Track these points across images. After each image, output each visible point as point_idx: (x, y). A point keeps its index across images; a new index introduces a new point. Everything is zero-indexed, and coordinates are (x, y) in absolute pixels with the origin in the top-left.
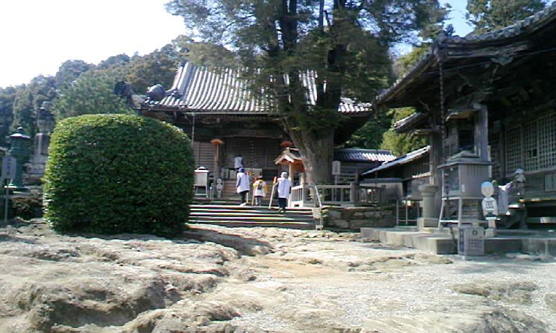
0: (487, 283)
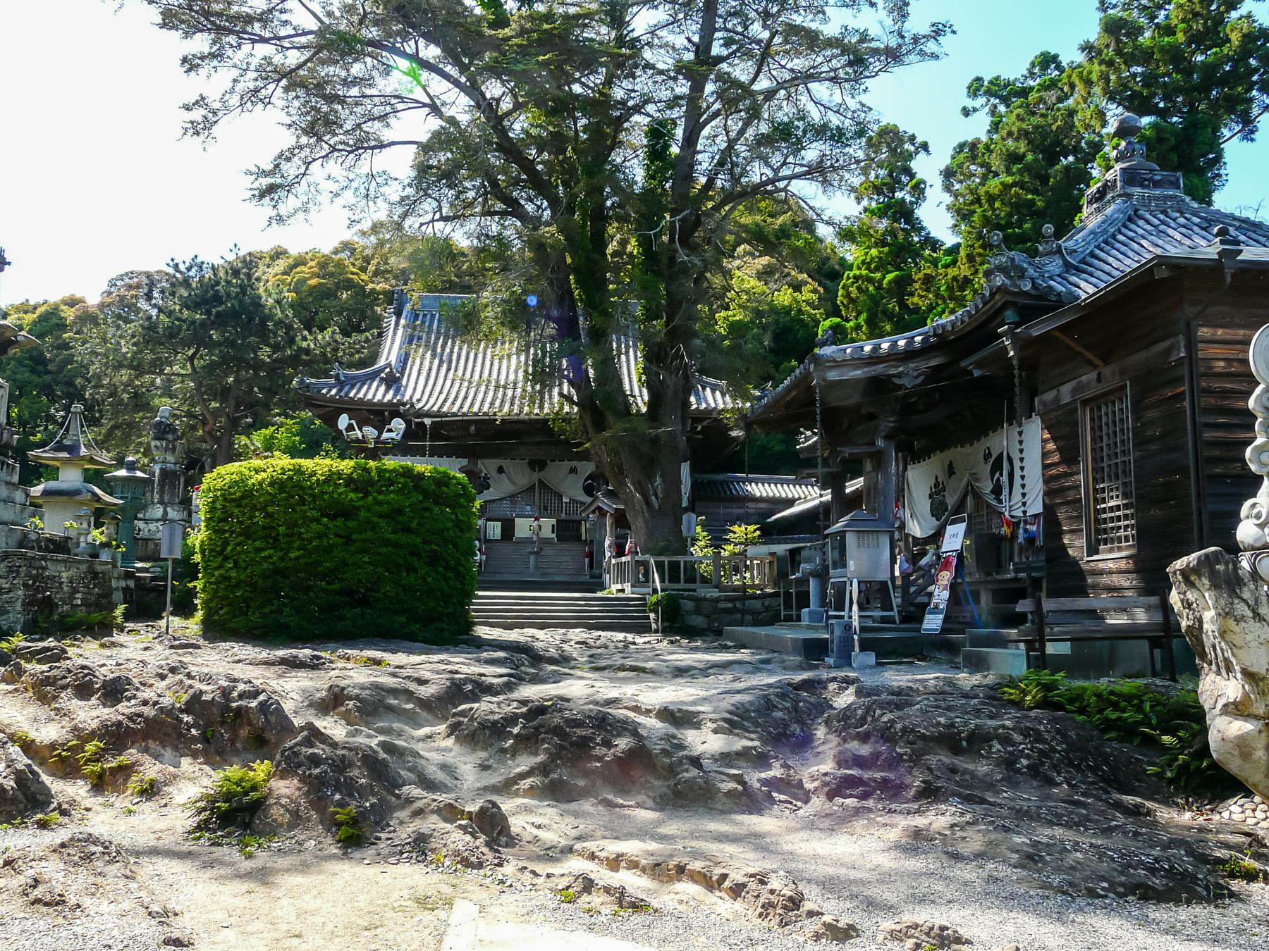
0: (247, 865)
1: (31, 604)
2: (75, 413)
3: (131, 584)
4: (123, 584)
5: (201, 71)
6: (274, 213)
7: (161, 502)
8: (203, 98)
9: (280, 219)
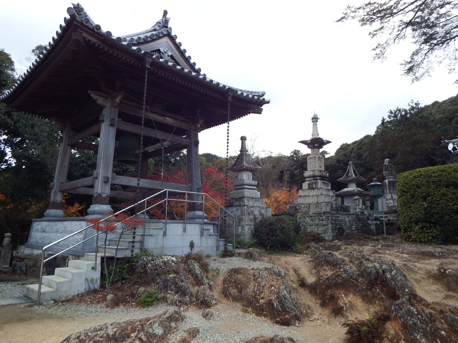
1: (335, 229)
2: (350, 164)
3: (378, 222)
4: (375, 222)
5: (377, 35)
6: (414, 77)
7: (390, 193)
8: (379, 44)
9: (417, 79)
